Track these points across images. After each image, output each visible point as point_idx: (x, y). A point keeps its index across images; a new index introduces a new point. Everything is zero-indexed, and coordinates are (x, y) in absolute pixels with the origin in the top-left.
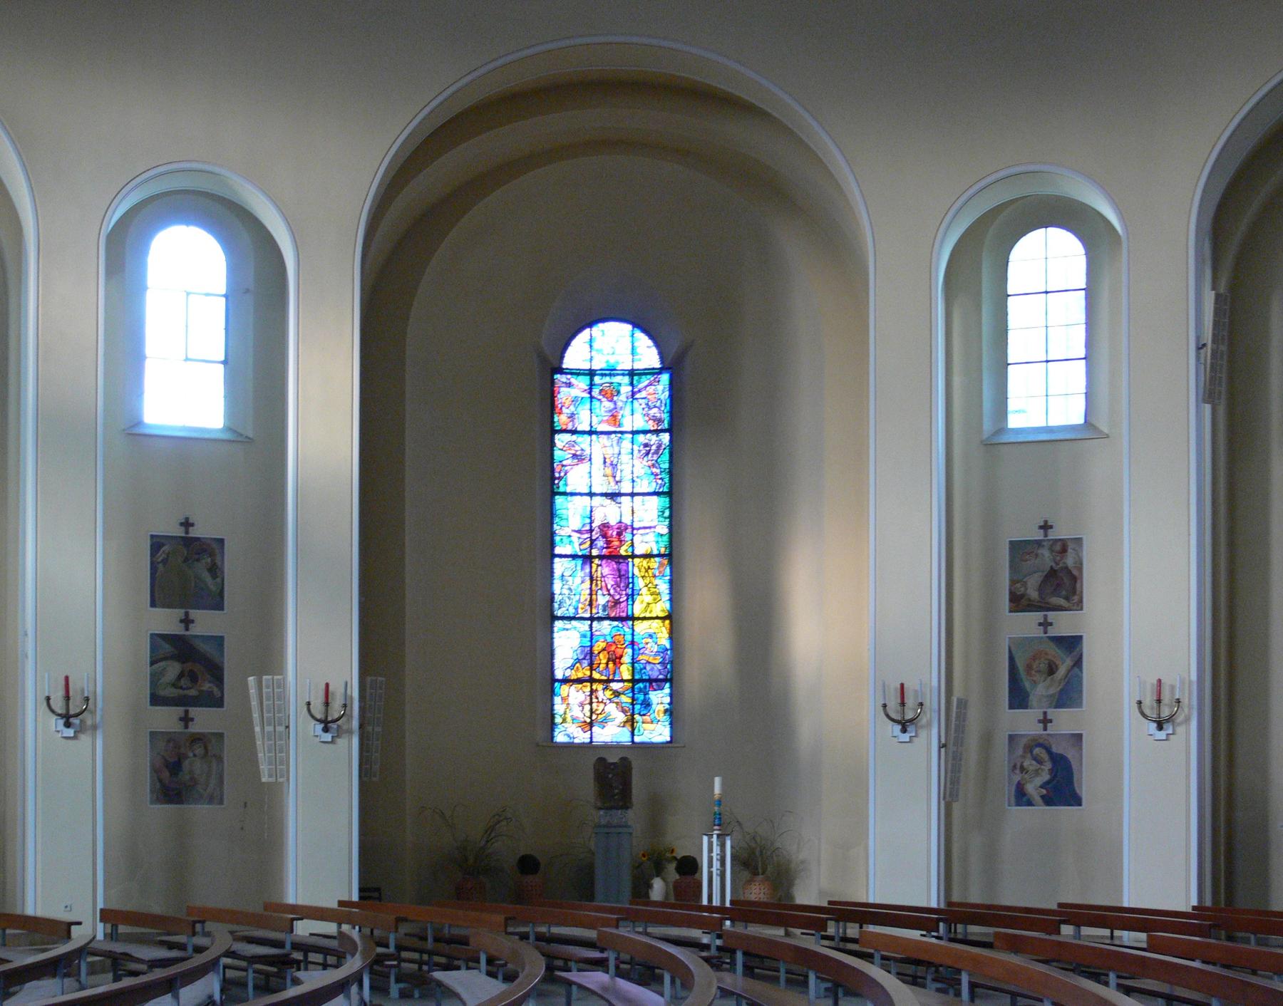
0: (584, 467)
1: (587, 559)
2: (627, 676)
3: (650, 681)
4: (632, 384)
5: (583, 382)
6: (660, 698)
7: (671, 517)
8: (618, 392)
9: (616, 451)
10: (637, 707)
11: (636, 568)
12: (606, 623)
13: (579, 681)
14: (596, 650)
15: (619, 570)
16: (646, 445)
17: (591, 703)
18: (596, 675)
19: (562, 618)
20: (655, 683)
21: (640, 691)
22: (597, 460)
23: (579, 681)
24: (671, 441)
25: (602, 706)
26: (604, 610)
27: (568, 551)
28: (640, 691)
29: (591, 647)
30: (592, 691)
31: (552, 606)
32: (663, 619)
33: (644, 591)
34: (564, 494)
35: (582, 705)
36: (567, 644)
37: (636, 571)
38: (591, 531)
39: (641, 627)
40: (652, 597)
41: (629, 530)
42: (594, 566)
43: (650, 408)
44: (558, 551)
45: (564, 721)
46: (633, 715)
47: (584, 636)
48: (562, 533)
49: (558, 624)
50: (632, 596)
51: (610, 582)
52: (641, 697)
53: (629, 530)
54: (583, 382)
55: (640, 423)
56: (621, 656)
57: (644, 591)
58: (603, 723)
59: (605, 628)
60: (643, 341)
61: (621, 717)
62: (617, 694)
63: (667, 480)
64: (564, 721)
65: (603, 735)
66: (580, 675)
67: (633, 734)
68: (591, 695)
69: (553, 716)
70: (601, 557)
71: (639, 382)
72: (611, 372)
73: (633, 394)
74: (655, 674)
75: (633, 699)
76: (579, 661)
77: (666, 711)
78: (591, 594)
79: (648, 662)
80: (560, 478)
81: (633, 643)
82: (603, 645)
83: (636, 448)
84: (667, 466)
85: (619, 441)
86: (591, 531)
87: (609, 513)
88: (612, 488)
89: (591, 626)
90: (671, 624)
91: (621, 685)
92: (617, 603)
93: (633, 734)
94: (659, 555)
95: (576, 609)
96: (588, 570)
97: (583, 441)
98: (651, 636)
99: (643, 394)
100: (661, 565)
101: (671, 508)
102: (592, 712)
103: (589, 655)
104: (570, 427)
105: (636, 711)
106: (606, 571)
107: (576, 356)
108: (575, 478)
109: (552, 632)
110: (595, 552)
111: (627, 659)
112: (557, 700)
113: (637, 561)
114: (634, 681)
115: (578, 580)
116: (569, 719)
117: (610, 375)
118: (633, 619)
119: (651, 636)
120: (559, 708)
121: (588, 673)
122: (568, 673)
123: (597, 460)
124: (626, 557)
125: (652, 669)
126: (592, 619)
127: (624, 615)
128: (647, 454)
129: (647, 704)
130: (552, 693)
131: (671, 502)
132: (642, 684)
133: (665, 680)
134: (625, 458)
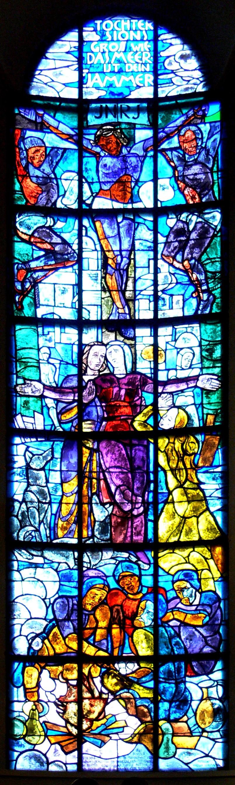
0: (66, 276)
1: (73, 440)
2: (144, 649)
3: (188, 658)
4: (153, 125)
5: (67, 123)
6: (205, 689)
7: (224, 360)
8: (131, 140)
9: (126, 245)
10: (164, 706)
11: (163, 454)
12: (107, 555)
13: (58, 659)
14: (89, 603)
15: (131, 459)
16: (178, 233)
17: (79, 701)
18: (90, 650)
19: (28, 546)
20: (200, 663)
21: (169, 676)
22: (92, 259)
23: (58, 659)
24: (223, 221)
25: (98, 707)
26: (103, 532)
27: (39, 423)
28: (169, 676)
29: (81, 597)
30: (82, 679)
31: (10, 524)
32: (210, 544)
33: (177, 495)
34: (35, 322)
35: (62, 704)
36: (36, 590)
37: (162, 460)
38: (80, 388)
39: (169, 561)
40: (190, 512)
41: (150, 387)
42: (86, 453)
43: (187, 166)
44: (19, 423)
45: (30, 731)
46: (156, 720)
47: (65, 578)
48: (28, 391)
49: (21, 556)
50: (154, 508)
51: (115, 482)
52: (171, 688)
53: (150, 387)
54: (67, 123)
55: (169, 195)
56: (135, 614)
57: (177, 495)
58: (102, 738)
59: (106, 563)
60: (174, 47)
61: (134, 724)
62: (126, 682)
63: (217, 293)
64: (30, 731)
65: (101, 757)
66: (60, 648)
67: (155, 757)
68: (79, 686)
69: (10, 723)
70: (95, 436)
71: (167, 121)
72: (117, 103)
73: (157, 141)
74: (196, 646)
75: (156, 690)
76: (57, 622)
77: (216, 712)
78: (79, 503)
79: (184, 624)
80: (24, 293)
81: (156, 589)
82: (100, 594)
83: (161, 239)
84: (217, 266)
85: (131, 231)
86: (80, 388)
87: (114, 356)
88: (118, 312)
89: (79, 561)
90: (225, 554)
91: (132, 667)
92: (127, 518)
93: (155, 757)
94: (204, 429)
95: (53, 529)
96: (74, 460)
97: (67, 229)
98: (188, 577)
99: (175, 142)
100: (207, 446)
101: (224, 343)
102: (81, 715)
103: (73, 613)
104: (42, 202)
105: (162, 714)
106: (108, 461)
107: (55, 75)
108: (54, 293)
109: (9, 569)
110: (87, 427)
111: (146, 619)
112: (18, 694)
113: (162, 442)
114: (156, 659)
115: (55, 478)
116: (39, 729)
117: (115, 111)
118: (157, 546)
119: (188, 577)
120: (21, 708)
121: (74, 645)
122: (37, 644)
123: (92, 259)
124: (145, 435)
125: (191, 637)
126: (81, 548)
127: (139, 539)
128: (181, 248)
129: (182, 701)
130: (9, 682)
131: (225, 333)
132: (171, 663)
133: (214, 657)
134: (142, 258)
